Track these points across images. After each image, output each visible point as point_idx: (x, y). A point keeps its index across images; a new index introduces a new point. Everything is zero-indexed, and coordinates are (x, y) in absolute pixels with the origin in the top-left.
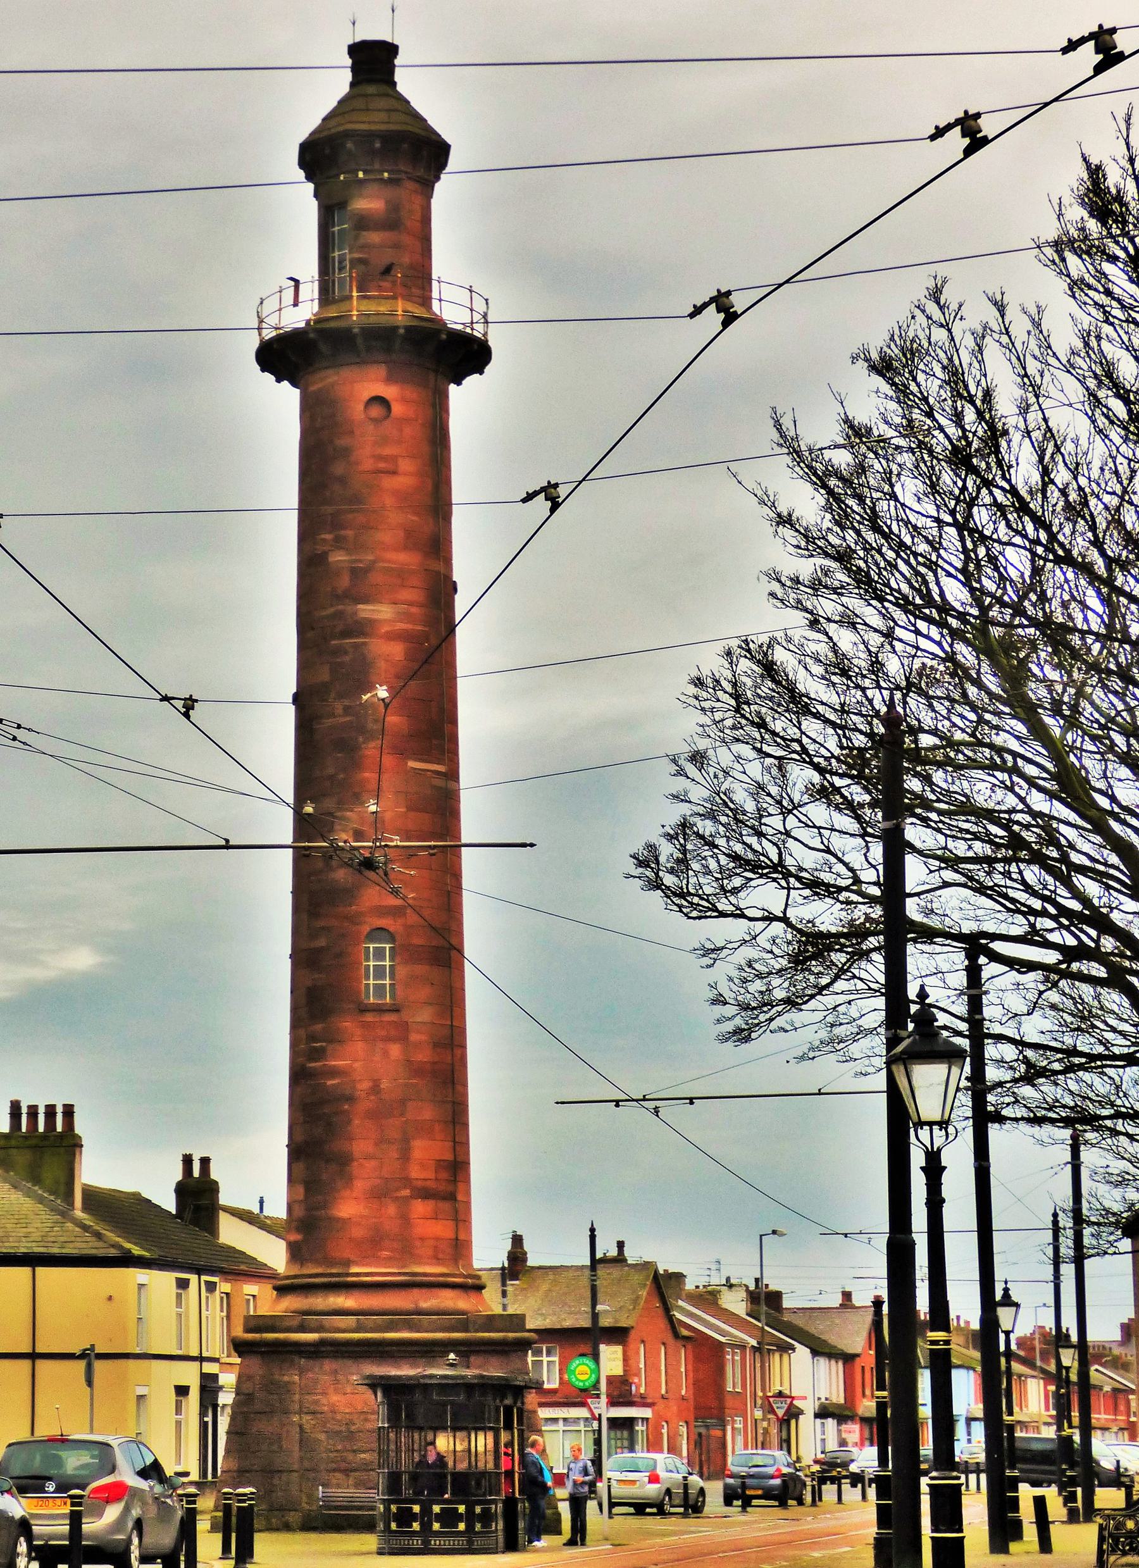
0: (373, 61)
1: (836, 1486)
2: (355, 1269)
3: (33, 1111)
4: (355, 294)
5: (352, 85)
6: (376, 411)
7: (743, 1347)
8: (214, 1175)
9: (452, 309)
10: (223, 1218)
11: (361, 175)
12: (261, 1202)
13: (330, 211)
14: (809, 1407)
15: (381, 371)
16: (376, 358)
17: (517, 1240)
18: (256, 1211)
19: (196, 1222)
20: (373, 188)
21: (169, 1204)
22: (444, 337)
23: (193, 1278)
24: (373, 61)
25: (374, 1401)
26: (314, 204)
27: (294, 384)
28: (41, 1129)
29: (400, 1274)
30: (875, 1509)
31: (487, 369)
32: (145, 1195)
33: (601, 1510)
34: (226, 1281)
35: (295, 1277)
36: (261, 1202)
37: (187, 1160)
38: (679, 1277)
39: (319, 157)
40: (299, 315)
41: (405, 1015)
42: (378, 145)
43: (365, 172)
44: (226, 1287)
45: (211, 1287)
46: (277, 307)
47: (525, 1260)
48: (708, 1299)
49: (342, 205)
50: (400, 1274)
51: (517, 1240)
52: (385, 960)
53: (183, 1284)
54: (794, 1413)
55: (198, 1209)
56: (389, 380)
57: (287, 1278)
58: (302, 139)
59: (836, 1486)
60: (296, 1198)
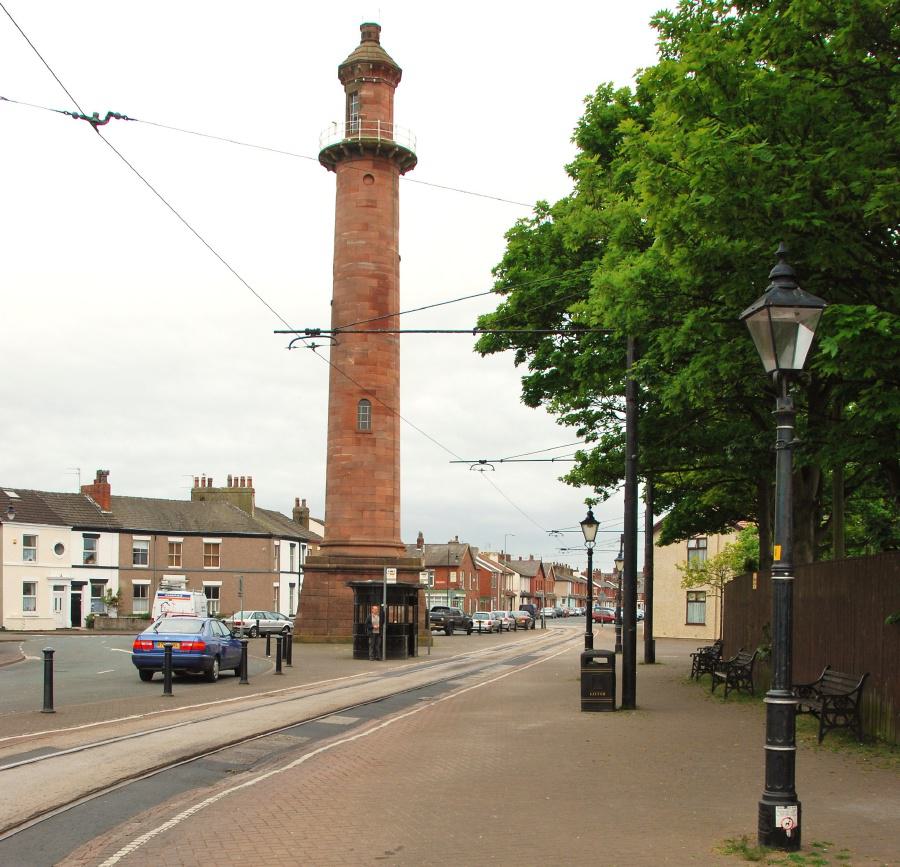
0: (370, 33)
1: (265, 640)
2: (352, 539)
3: (236, 480)
5: (362, 42)
6: (368, 181)
7: (497, 573)
9: (401, 138)
10: (311, 521)
13: (350, 96)
14: (518, 594)
15: (370, 163)
16: (369, 160)
17: (421, 535)
19: (301, 523)
20: (368, 85)
23: (297, 544)
24: (370, 33)
25: (350, 592)
26: (344, 95)
27: (334, 171)
30: (757, 808)
33: (268, 653)
37: (297, 500)
38: (477, 549)
39: (347, 73)
40: (338, 136)
41: (374, 436)
44: (311, 547)
45: (304, 547)
48: (485, 556)
49: (356, 93)
51: (421, 535)
53: (292, 546)
54: (514, 596)
55: (301, 518)
56: (375, 167)
59: (265, 640)
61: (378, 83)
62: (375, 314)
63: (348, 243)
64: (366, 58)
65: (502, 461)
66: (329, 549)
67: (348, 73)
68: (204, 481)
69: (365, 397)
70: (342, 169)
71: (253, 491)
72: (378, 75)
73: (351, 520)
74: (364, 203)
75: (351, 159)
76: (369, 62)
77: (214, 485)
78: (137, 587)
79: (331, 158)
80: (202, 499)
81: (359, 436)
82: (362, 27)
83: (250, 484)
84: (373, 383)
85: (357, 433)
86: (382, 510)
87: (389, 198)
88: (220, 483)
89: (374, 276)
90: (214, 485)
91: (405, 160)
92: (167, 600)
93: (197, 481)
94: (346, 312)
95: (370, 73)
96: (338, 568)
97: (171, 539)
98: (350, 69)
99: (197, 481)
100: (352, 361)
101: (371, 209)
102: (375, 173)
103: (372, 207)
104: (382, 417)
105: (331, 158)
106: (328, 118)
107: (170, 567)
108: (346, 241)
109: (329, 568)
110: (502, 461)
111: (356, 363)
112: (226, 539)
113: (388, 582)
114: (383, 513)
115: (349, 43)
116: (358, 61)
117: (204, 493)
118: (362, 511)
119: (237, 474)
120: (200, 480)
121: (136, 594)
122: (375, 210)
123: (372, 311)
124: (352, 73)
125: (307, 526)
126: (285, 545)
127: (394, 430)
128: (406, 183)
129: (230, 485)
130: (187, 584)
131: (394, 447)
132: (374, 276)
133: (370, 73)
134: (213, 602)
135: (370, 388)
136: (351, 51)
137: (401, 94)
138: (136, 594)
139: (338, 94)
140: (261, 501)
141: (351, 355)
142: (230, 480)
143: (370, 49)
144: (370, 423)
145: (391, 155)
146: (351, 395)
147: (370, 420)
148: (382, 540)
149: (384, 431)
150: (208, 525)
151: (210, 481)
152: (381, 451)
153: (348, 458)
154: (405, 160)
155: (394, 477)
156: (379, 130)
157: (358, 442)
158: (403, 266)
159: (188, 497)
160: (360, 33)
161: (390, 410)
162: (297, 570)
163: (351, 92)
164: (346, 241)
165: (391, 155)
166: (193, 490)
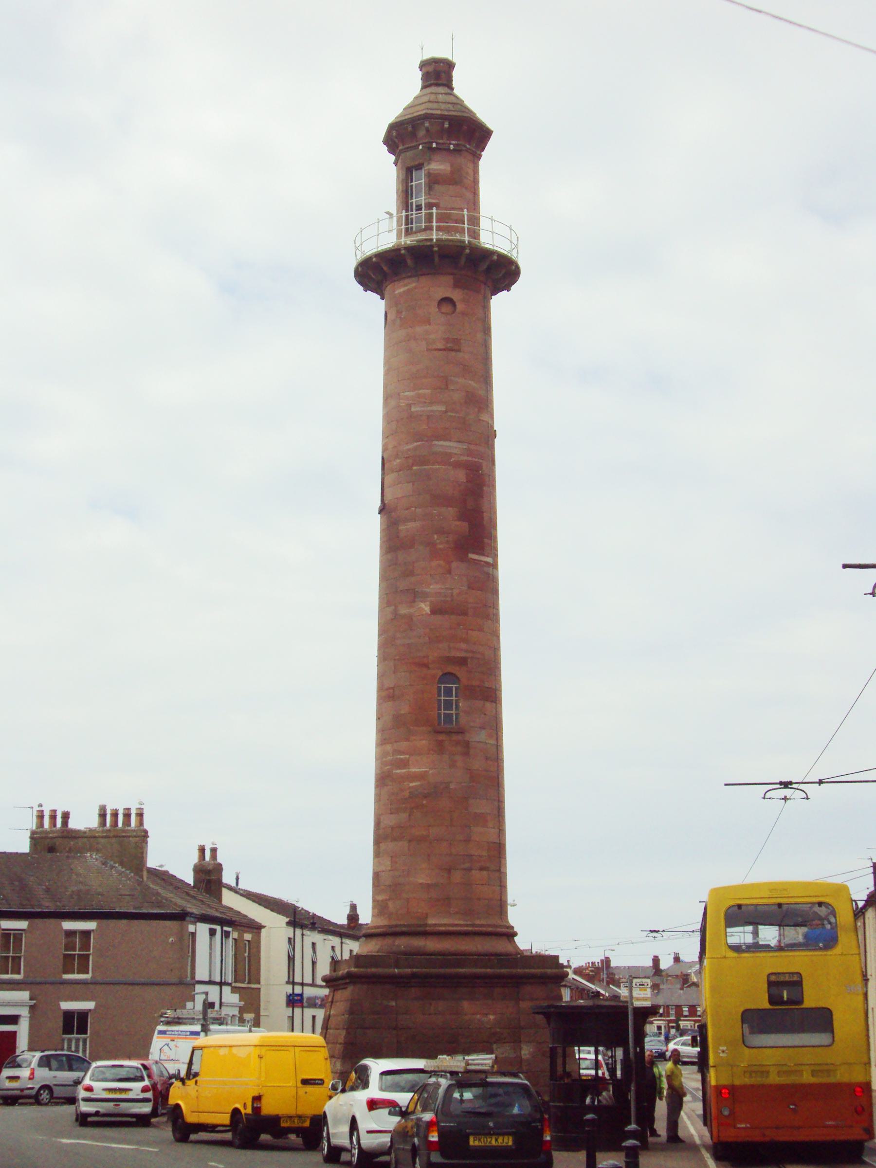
0: (438, 73)
3: (115, 815)
4: (434, 224)
6: (447, 308)
8: (220, 860)
9: (492, 237)
11: (434, 145)
12: (237, 879)
13: (408, 172)
15: (448, 280)
17: (353, 907)
18: (233, 884)
21: (189, 878)
22: (495, 257)
23: (218, 928)
24: (438, 73)
28: (120, 824)
29: (467, 925)
31: (513, 287)
32: (171, 872)
34: (237, 930)
35: (396, 926)
36: (237, 879)
37: (202, 850)
39: (401, 137)
40: (386, 237)
41: (467, 737)
42: (446, 125)
43: (437, 144)
44: (235, 935)
45: (227, 935)
46: (376, 233)
47: (358, 919)
50: (467, 925)
52: (452, 696)
53: (212, 933)
55: (209, 882)
56: (457, 285)
57: (372, 928)
58: (391, 119)
60: (383, 868)
61: (458, 151)
62: (464, 526)
63: (413, 409)
64: (439, 112)
65: (820, 782)
66: (389, 941)
67: (401, 137)
68: (53, 817)
69: (450, 669)
70: (400, 288)
71: (145, 835)
72: (457, 139)
73: (429, 886)
74: (440, 346)
75: (416, 273)
76: (443, 118)
77: (73, 824)
78: (68, 1015)
79: (375, 273)
80: (51, 849)
81: (441, 737)
82: (423, 65)
83: (141, 822)
84: (463, 646)
85: (438, 732)
86: (482, 869)
87: (480, 336)
88: (84, 820)
89: (457, 465)
90: (73, 824)
91: (501, 272)
92: (168, 1041)
93: (41, 816)
94: (411, 525)
95: (439, 139)
96: (413, 976)
97: (69, 925)
98: (410, 129)
99: (41, 816)
100: (426, 608)
101: (453, 354)
102: (456, 295)
103: (451, 350)
104: (479, 703)
105: (375, 273)
106: (371, 210)
107: (66, 977)
108: (410, 406)
109: (400, 976)
110: (820, 782)
111: (433, 612)
112: (105, 922)
113: (637, 1004)
114: (485, 873)
115: (404, 92)
116: (427, 117)
117: (55, 841)
118: (449, 871)
119: (117, 803)
120: (133, 812)
121: (68, 1029)
122: (461, 355)
123: (458, 523)
124: (414, 135)
125: (219, 898)
126: (202, 930)
127: (495, 726)
128: (500, 304)
129: (103, 822)
130: (32, 1008)
131: (495, 758)
132: (457, 465)
133: (439, 139)
134: (78, 1040)
135: (459, 654)
136: (408, 100)
137: (491, 165)
138: (68, 1029)
139: (385, 169)
140: (156, 857)
141: (424, 596)
142: (103, 815)
143: (433, 97)
144: (439, 709)
145: (484, 266)
146: (426, 666)
147: (439, 715)
148: (483, 922)
149: (482, 728)
150: (71, 896)
151: (66, 816)
152: (477, 764)
153: (421, 776)
154: (501, 272)
155: (499, 812)
156: (466, 226)
157: (440, 748)
158: (499, 444)
159: (23, 846)
160: (419, 74)
161: (490, 694)
162: (319, 982)
163: (410, 164)
164: (410, 406)
165: (484, 266)
166: (33, 833)
